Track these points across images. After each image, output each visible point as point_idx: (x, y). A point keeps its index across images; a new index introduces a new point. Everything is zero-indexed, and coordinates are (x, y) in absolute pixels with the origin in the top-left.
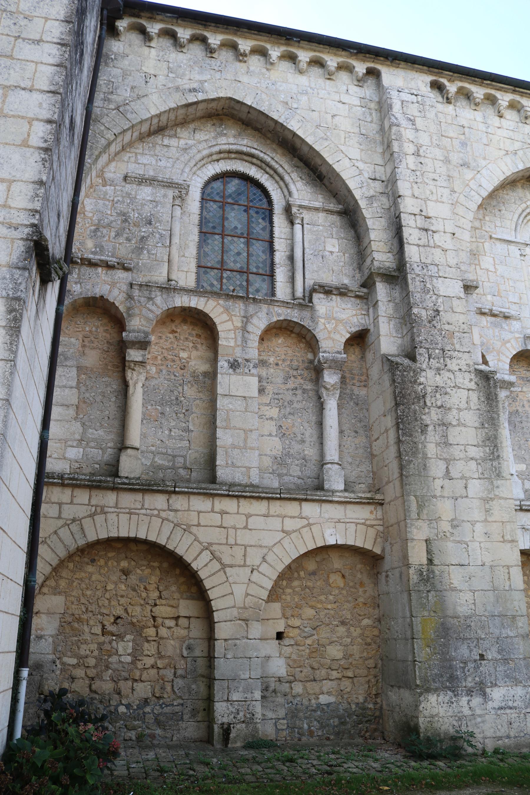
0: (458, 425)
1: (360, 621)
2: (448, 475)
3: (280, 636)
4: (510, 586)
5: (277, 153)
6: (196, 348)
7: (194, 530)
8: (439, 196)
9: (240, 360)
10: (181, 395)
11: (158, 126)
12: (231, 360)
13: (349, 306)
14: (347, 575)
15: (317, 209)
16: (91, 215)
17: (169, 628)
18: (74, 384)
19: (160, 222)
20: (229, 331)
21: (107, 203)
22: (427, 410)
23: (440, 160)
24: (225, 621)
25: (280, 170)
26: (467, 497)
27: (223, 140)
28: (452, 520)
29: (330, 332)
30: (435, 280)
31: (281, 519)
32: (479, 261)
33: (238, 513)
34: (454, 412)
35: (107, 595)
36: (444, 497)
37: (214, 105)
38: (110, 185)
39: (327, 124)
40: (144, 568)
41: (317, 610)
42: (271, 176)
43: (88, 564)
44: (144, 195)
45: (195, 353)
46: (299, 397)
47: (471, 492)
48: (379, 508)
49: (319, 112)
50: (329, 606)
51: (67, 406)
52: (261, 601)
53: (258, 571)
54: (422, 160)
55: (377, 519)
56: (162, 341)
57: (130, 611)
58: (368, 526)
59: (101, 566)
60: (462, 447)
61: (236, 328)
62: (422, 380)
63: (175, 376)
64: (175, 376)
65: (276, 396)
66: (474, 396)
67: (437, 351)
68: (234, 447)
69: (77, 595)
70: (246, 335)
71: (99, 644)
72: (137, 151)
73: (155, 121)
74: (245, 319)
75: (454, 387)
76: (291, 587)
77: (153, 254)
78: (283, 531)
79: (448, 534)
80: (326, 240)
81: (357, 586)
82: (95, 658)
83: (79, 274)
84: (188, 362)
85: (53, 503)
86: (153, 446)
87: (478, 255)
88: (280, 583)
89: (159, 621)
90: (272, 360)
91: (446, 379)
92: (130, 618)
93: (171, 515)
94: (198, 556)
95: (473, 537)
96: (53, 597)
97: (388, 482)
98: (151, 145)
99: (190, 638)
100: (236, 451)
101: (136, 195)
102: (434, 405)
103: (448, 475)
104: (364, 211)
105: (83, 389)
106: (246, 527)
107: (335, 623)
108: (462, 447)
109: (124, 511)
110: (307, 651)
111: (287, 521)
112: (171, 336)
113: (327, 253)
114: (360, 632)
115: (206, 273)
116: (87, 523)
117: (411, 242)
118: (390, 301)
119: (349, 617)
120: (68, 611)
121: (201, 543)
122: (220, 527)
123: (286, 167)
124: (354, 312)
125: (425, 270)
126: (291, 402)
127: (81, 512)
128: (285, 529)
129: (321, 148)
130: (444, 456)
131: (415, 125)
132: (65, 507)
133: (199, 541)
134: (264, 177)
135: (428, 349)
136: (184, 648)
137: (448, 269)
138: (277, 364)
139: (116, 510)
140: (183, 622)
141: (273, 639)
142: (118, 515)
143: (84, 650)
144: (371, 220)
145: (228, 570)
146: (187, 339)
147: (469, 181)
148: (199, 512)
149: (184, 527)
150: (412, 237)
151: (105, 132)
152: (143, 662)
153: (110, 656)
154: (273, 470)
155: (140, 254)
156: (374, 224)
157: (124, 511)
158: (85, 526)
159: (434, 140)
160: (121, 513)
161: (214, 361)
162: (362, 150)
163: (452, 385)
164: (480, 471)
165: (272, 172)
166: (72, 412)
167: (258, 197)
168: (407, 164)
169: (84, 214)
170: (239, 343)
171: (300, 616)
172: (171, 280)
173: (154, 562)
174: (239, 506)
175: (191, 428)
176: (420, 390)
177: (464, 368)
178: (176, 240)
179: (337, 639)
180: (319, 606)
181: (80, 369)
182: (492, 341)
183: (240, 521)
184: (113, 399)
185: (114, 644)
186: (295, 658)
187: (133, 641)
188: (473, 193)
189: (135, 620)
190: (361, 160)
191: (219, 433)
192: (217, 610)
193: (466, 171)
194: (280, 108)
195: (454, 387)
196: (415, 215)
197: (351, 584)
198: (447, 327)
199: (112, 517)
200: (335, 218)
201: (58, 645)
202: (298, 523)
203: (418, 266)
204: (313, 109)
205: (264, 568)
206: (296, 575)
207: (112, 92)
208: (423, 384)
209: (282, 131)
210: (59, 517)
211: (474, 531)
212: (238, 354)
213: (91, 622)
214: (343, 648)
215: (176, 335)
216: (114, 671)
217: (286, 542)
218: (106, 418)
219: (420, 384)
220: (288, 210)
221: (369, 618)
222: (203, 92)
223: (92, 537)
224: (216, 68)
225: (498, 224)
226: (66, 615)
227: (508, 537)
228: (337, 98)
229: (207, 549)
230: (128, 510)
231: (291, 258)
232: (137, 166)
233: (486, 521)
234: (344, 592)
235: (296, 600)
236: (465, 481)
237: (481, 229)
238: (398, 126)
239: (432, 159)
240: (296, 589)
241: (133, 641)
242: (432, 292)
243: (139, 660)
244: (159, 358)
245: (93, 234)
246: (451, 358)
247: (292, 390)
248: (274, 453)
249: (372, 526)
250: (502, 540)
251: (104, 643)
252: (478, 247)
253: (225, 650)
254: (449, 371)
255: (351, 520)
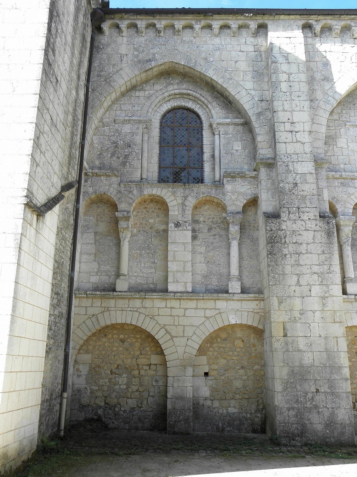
0: (307, 253)
1: (253, 367)
2: (298, 284)
3: (206, 374)
4: (338, 349)
5: (204, 91)
6: (158, 216)
7: (156, 318)
8: (302, 107)
9: (181, 222)
10: (150, 243)
11: (131, 86)
12: (176, 222)
13: (246, 183)
14: (245, 340)
15: (228, 124)
16: (97, 145)
17: (146, 370)
18: (93, 242)
19: (135, 145)
20: (175, 205)
21: (105, 137)
22: (286, 246)
23: (304, 82)
24: (173, 367)
25: (206, 102)
26: (310, 296)
27: (171, 88)
28: (300, 310)
29: (234, 201)
30: (295, 163)
31: (204, 310)
32: (336, 142)
33: (180, 308)
34: (304, 245)
35: (113, 353)
36: (295, 297)
37: (163, 67)
38: (107, 126)
39: (231, 68)
40: (132, 338)
41: (228, 360)
42: (201, 106)
43: (103, 337)
44: (126, 129)
45: (157, 219)
46: (217, 240)
47: (313, 293)
48: (262, 302)
49: (227, 61)
50: (234, 358)
51: (90, 254)
52: (192, 356)
53: (191, 339)
54: (291, 84)
55: (260, 309)
56: (139, 214)
57: (125, 362)
58: (255, 313)
59: (110, 338)
60: (309, 266)
61: (178, 204)
62: (284, 227)
63: (147, 233)
64: (147, 233)
65: (204, 240)
66: (318, 235)
67: (294, 209)
68: (177, 271)
69: (98, 354)
70: (184, 207)
71: (109, 379)
72: (121, 103)
73: (128, 84)
74: (184, 198)
75: (305, 230)
76: (213, 347)
77: (132, 165)
78: (205, 317)
79: (297, 319)
80: (234, 143)
81: (251, 347)
82: (107, 386)
83: (91, 181)
84: (154, 225)
85: (82, 307)
86: (135, 273)
87: (336, 138)
88: (206, 345)
89: (140, 366)
90: (201, 219)
91: (300, 225)
92: (125, 365)
93: (143, 310)
94: (158, 332)
95: (314, 320)
96: (85, 355)
97: (265, 288)
98: (129, 98)
99: (156, 376)
100: (179, 274)
101: (121, 130)
102: (291, 242)
103: (298, 284)
104: (254, 123)
105: (97, 244)
106: (184, 316)
107: (238, 367)
108: (309, 266)
109: (119, 309)
110: (222, 383)
111: (207, 311)
112: (145, 210)
113: (234, 151)
114: (253, 373)
115: (164, 171)
116: (100, 317)
117: (280, 141)
118: (269, 179)
119: (246, 364)
120: (93, 362)
121: (160, 325)
122: (171, 316)
123: (209, 99)
124: (249, 187)
125: (289, 158)
126: (212, 243)
127: (96, 311)
128: (206, 316)
129: (228, 85)
130: (297, 272)
131: (288, 60)
132: (89, 309)
133: (158, 324)
134: (197, 107)
135: (288, 208)
136: (153, 381)
137: (305, 155)
138: (204, 222)
139: (115, 309)
140: (153, 367)
141: (202, 376)
142: (116, 312)
143: (101, 382)
144: (259, 128)
145: (174, 339)
146: (153, 211)
147: (328, 90)
148: (159, 308)
149: (151, 316)
150: (282, 138)
151: (99, 96)
152: (132, 388)
153: (115, 385)
154: (202, 283)
155: (125, 166)
156: (260, 130)
157: (119, 309)
158: (99, 318)
159: (300, 68)
160: (117, 310)
161: (167, 224)
162: (254, 82)
163: (304, 229)
164: (320, 280)
165: (201, 103)
166: (92, 257)
167: (194, 120)
168: (281, 89)
169: (93, 145)
170: (180, 212)
171: (217, 364)
172: (143, 179)
173: (137, 335)
174: (180, 304)
175: (156, 261)
176: (282, 234)
177: (312, 218)
178: (145, 154)
179: (239, 377)
180: (229, 358)
181: (96, 233)
182: (341, 195)
183: (180, 312)
184: (114, 249)
185: (117, 379)
186: (215, 387)
187: (127, 377)
188: (330, 98)
189: (127, 366)
190: (254, 89)
191: (170, 264)
192: (169, 361)
193: (326, 83)
194: (202, 62)
195: (305, 230)
196: (284, 123)
197: (248, 345)
198: (302, 193)
199: (113, 313)
200: (240, 128)
201: (89, 380)
202: (214, 312)
203: (284, 156)
204: (223, 59)
205: (194, 338)
206: (215, 340)
207: (102, 71)
208: (284, 230)
209: (204, 77)
210: (86, 314)
211: (314, 317)
212: (180, 219)
213: (105, 368)
214: (242, 381)
215: (147, 209)
216: (117, 393)
217: (207, 323)
218: (111, 259)
219: (282, 230)
220: (211, 126)
221: (258, 365)
222: (155, 61)
223: (103, 324)
224: (162, 43)
225: (352, 114)
226: (92, 364)
227: (337, 320)
228: (239, 49)
229: (163, 328)
230: (121, 309)
231: (213, 156)
232: (121, 111)
233: (323, 310)
234: (243, 350)
235: (215, 354)
236: (309, 287)
237: (339, 120)
238: (276, 63)
239: (298, 82)
240: (215, 349)
241: (127, 377)
242: (293, 172)
243: (130, 387)
244: (138, 224)
245: (98, 157)
246: (303, 212)
247: (213, 236)
248: (203, 272)
249: (258, 313)
250: (333, 321)
251: (112, 378)
252: (336, 133)
253: (173, 382)
254: (302, 220)
255: (245, 310)
